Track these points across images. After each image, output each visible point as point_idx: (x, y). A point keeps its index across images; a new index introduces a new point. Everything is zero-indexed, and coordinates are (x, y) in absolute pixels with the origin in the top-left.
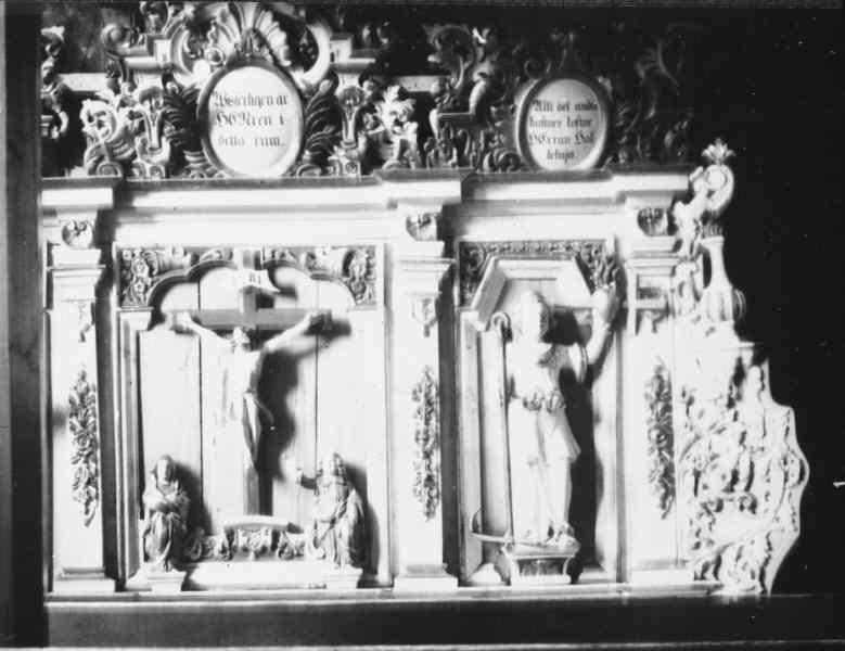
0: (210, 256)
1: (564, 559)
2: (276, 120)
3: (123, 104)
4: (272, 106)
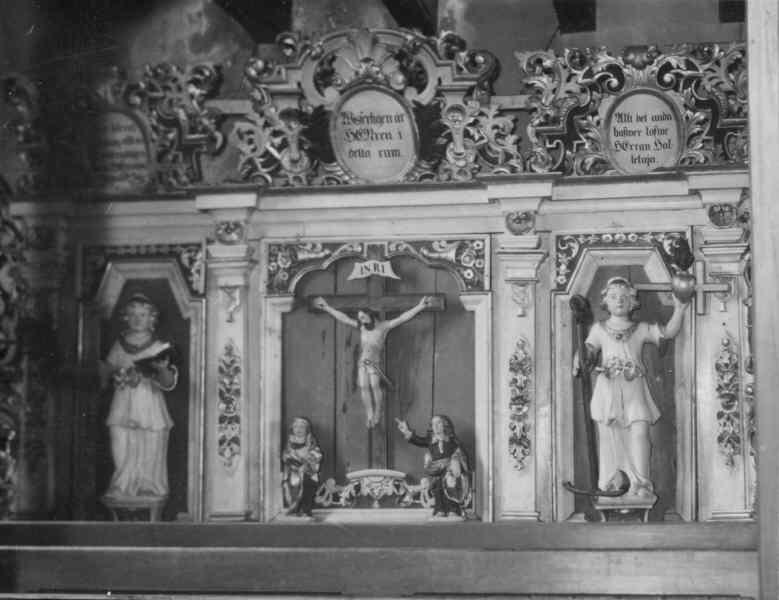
0: (345, 251)
1: (644, 510)
2: (395, 135)
3: (267, 125)
4: (391, 124)
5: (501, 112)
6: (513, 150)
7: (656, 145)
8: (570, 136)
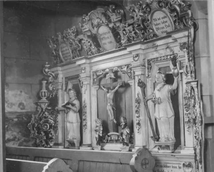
5: (129, 25)
6: (134, 35)
7: (166, 26)
8: (145, 29)
